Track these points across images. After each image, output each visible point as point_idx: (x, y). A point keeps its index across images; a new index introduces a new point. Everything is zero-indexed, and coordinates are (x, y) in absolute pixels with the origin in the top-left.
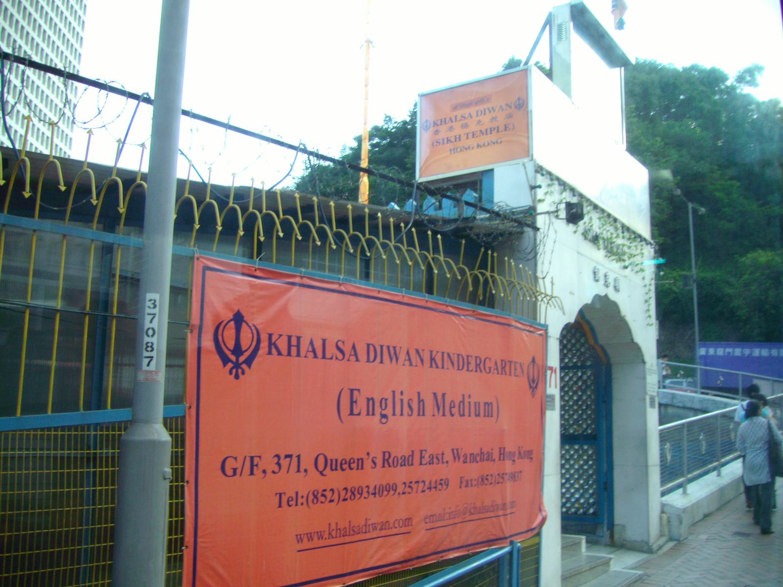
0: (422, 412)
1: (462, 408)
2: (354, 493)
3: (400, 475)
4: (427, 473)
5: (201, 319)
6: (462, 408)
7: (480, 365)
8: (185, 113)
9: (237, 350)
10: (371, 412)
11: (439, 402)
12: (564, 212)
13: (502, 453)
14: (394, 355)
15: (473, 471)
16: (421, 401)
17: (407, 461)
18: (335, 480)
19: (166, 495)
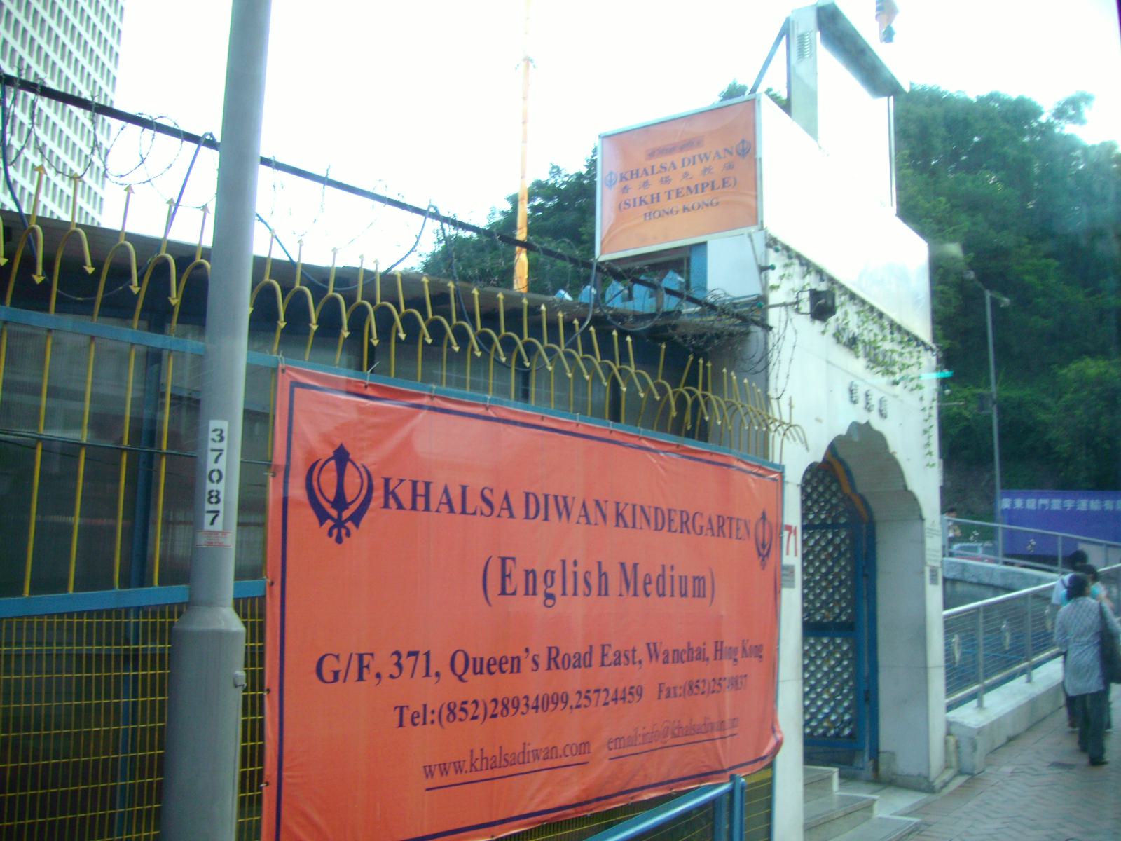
0: (604, 591)
1: (661, 585)
2: (507, 706)
3: (573, 680)
4: (611, 677)
5: (288, 458)
6: (661, 585)
7: (687, 523)
8: (265, 162)
9: (340, 502)
10: (531, 591)
11: (629, 577)
12: (808, 304)
13: (719, 649)
14: (564, 509)
15: (677, 674)
16: (602, 575)
17: (582, 661)
18: (480, 687)
19: (238, 709)
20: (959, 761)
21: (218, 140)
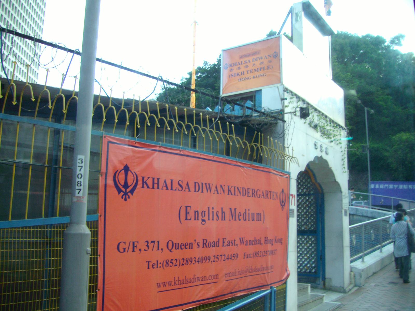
0: (223, 219)
1: (245, 216)
2: (188, 261)
3: (212, 252)
4: (226, 250)
5: (107, 169)
6: (245, 216)
7: (254, 193)
8: (98, 60)
9: (126, 185)
10: (196, 218)
11: (233, 213)
12: (299, 112)
13: (266, 240)
14: (209, 188)
15: (251, 249)
16: (223, 213)
17: (216, 244)
18: (178, 254)
19: (88, 262)
20: (355, 281)
21: (81, 52)
